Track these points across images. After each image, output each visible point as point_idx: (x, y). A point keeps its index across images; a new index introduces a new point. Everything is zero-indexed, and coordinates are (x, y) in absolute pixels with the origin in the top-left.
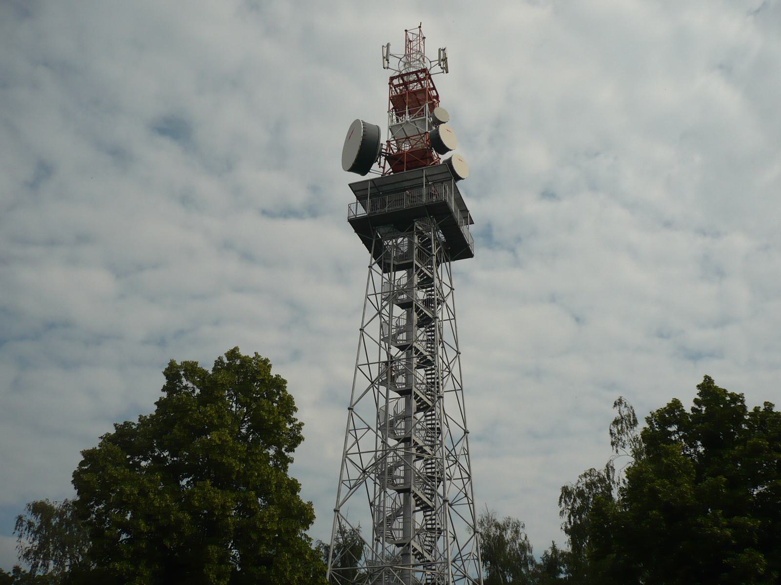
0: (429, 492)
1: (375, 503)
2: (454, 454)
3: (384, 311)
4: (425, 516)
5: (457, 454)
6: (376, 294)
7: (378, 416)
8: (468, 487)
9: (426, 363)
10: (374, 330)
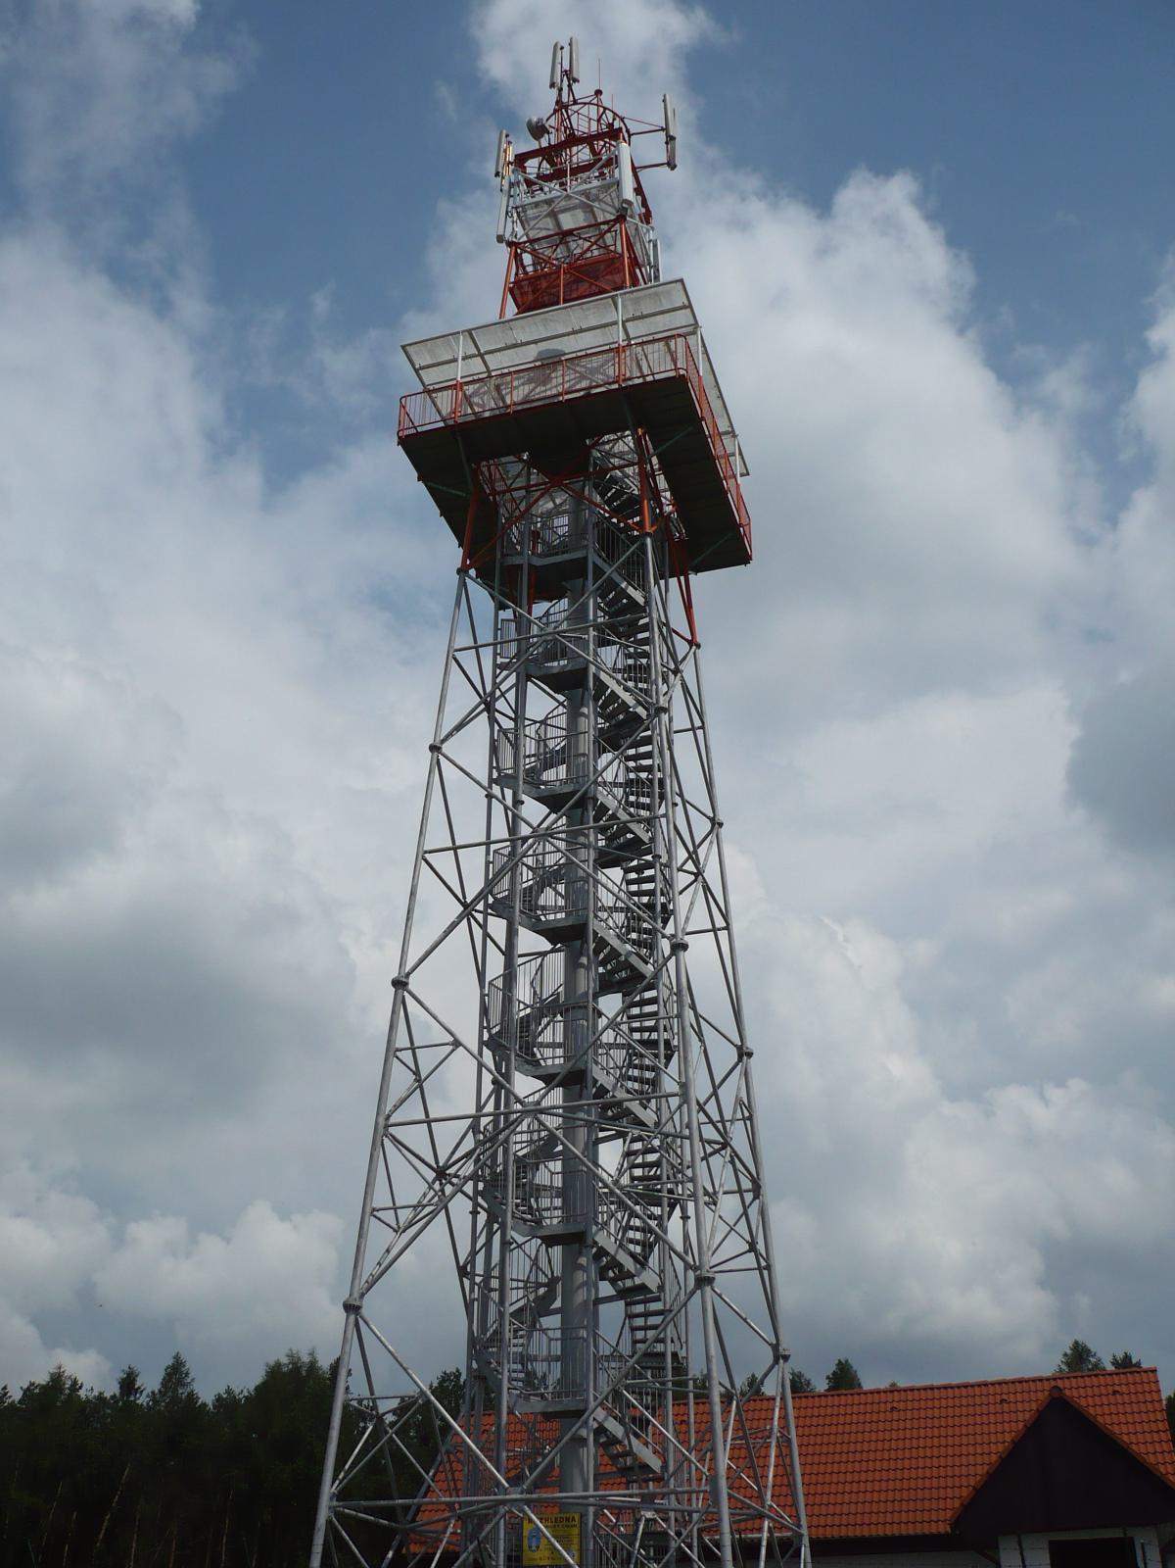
0: (638, 1236)
1: (473, 1267)
2: (716, 1117)
3: (500, 705)
4: (630, 1316)
5: (726, 1118)
6: (476, 648)
7: (484, 1011)
8: (753, 1211)
9: (626, 980)
10: (472, 749)
